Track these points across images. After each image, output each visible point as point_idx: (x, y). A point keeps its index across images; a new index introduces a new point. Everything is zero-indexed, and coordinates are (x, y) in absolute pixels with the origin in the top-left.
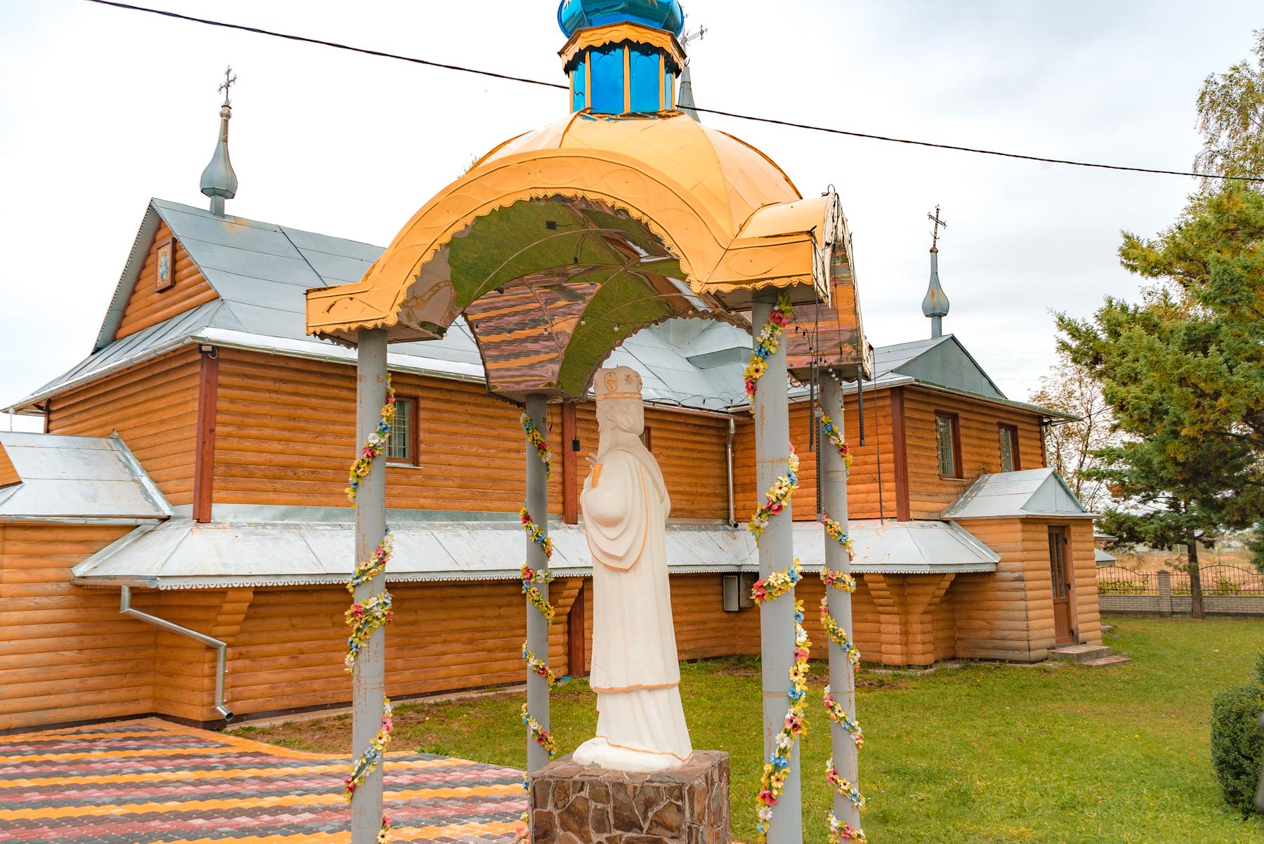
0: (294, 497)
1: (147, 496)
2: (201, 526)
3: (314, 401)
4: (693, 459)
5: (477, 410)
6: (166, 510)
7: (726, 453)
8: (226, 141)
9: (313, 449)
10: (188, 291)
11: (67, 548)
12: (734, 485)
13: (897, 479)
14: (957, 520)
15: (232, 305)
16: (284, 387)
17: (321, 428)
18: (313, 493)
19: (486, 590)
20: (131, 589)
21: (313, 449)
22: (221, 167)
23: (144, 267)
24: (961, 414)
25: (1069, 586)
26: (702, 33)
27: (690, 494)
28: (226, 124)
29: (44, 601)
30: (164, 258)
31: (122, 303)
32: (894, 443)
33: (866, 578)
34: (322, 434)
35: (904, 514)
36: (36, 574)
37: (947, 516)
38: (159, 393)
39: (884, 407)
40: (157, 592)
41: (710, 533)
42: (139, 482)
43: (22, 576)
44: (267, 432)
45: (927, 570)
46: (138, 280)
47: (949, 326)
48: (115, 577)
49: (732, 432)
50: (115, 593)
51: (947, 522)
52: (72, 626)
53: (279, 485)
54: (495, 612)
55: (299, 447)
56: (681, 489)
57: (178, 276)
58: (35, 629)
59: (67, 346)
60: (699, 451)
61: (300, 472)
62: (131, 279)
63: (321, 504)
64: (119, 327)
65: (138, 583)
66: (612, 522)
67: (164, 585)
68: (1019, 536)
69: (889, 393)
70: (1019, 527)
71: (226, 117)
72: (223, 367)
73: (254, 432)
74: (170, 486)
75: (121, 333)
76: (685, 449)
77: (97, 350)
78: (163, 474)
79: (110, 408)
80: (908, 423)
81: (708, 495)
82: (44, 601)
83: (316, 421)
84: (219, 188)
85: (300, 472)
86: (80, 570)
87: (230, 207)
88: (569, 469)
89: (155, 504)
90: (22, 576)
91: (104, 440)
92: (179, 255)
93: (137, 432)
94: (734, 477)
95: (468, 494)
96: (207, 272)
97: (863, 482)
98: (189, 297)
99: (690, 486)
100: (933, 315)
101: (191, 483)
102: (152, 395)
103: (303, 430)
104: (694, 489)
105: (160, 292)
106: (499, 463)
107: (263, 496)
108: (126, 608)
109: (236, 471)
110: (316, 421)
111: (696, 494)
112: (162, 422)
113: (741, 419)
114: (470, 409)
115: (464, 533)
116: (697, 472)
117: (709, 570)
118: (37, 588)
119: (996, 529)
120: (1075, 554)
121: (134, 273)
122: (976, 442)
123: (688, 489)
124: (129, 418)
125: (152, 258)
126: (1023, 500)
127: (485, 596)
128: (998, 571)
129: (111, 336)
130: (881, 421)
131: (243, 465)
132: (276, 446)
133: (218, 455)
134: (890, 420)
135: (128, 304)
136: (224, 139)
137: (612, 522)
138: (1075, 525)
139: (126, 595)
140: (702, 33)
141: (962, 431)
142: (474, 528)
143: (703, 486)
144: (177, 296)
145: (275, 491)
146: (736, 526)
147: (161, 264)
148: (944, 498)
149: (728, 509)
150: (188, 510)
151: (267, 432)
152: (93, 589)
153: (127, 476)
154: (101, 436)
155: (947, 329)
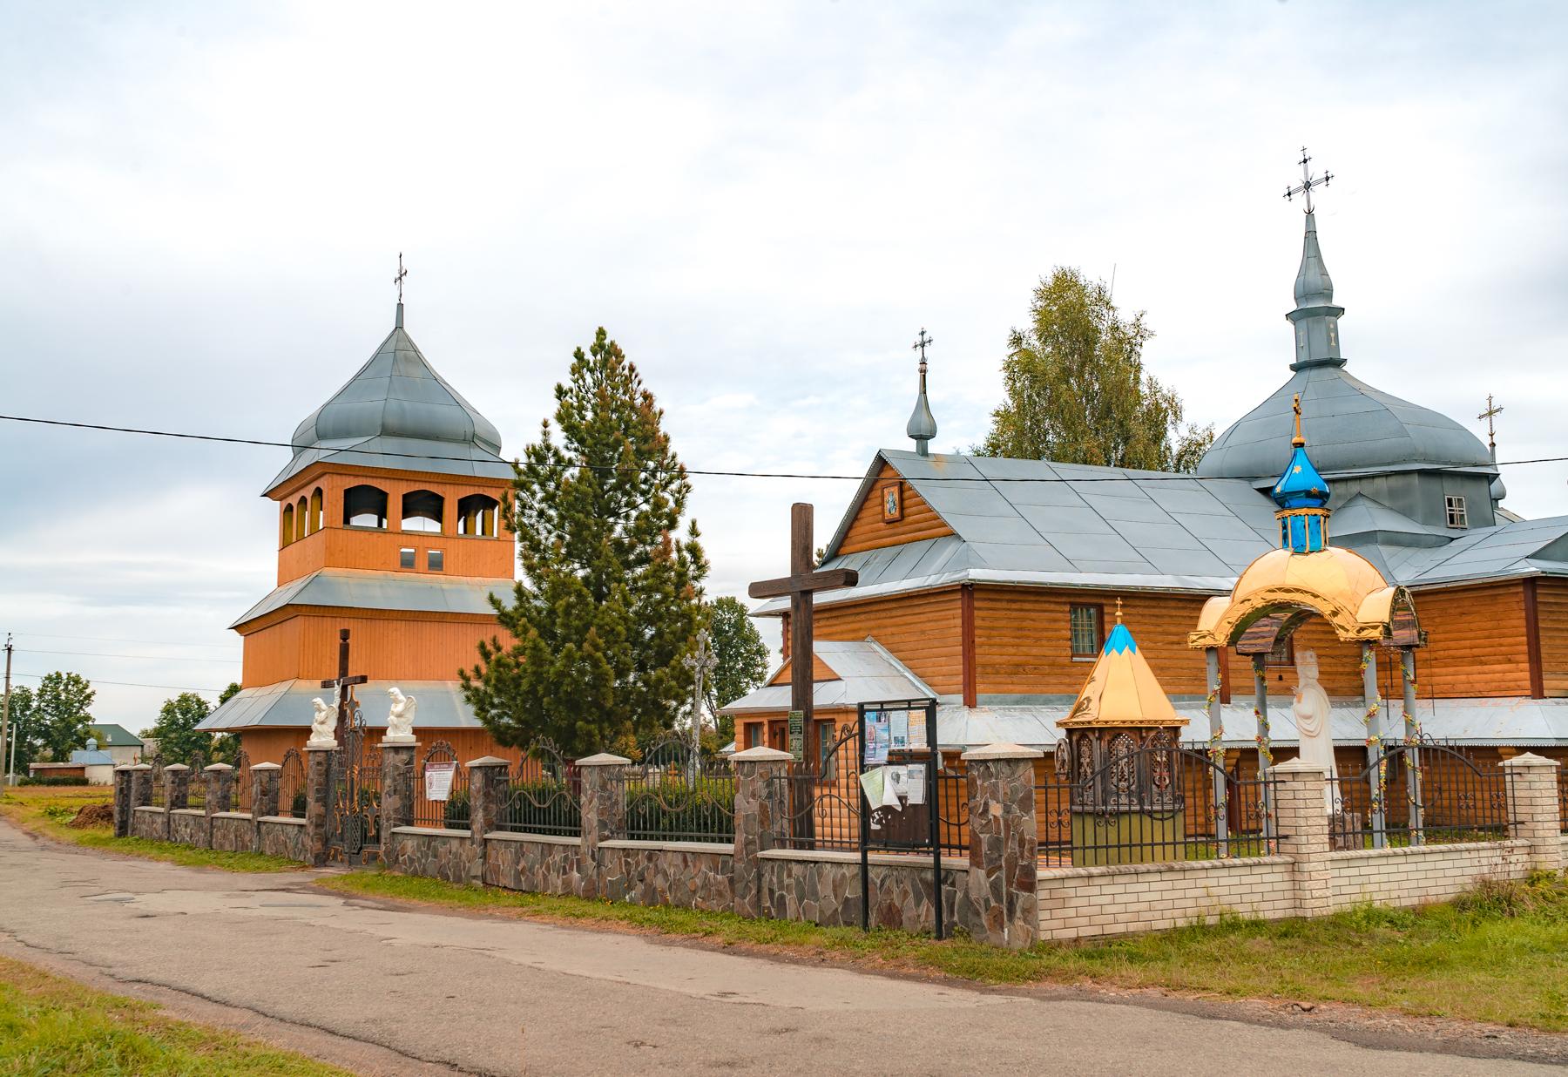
3: (1033, 615)
5: (1146, 611)
9: (1035, 651)
13: (1530, 661)
16: (1014, 606)
17: (1038, 635)
21: (1035, 651)
30: (891, 496)
32: (1527, 627)
34: (1039, 639)
35: (1538, 693)
38: (917, 610)
44: (1006, 640)
45: (1553, 743)
53: (1015, 679)
57: (907, 511)
71: (923, 372)
72: (976, 595)
73: (997, 640)
74: (937, 680)
75: (843, 550)
80: (1541, 608)
84: (922, 436)
87: (933, 446)
92: (907, 494)
93: (896, 639)
97: (1499, 663)
103: (1028, 637)
105: (889, 523)
106: (1165, 654)
109: (989, 670)
111: (1337, 673)
114: (1141, 611)
117: (1351, 744)
130: (1515, 606)
131: (993, 665)
132: (1012, 650)
133: (978, 659)
144: (901, 530)
151: (1006, 640)
154: (853, 640)
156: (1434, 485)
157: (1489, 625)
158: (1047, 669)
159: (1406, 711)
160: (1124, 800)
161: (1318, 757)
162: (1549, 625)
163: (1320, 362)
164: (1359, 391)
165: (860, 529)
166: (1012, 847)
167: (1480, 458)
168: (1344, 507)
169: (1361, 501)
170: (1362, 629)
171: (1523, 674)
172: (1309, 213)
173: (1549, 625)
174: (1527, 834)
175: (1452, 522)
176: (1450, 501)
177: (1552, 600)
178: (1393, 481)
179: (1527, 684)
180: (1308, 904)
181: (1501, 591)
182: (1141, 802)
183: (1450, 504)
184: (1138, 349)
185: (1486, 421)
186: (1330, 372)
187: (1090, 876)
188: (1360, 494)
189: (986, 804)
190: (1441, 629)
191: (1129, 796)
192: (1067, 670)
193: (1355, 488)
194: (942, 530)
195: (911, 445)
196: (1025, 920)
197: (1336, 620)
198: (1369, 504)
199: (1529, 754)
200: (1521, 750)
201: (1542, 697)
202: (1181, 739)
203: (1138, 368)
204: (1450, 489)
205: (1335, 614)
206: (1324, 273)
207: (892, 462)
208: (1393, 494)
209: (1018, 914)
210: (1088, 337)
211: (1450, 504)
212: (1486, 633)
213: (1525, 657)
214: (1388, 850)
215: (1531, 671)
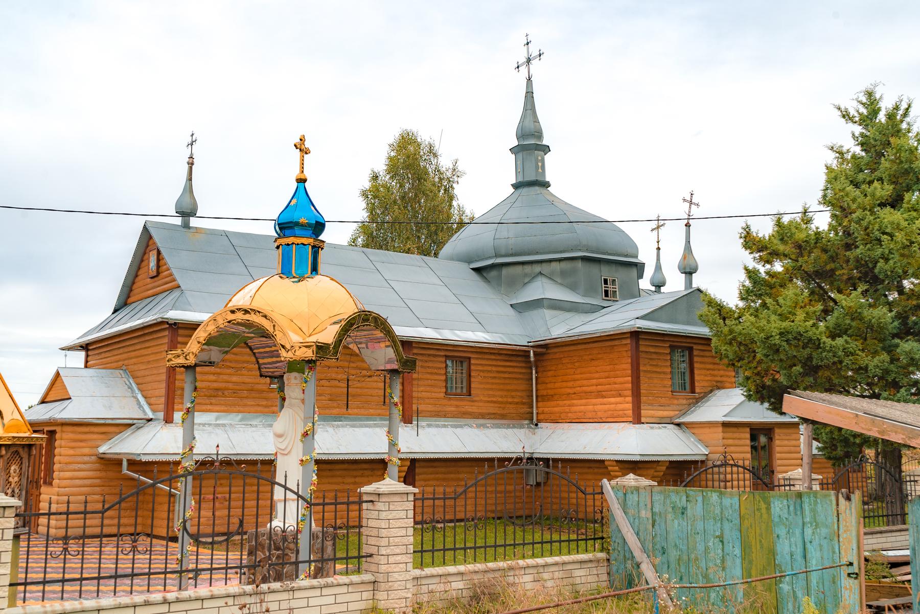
0: (223, 408)
1: (140, 406)
2: (168, 425)
4: (505, 378)
6: (150, 415)
7: (532, 373)
8: (190, 179)
9: (234, 379)
10: (167, 279)
11: (95, 436)
12: (537, 396)
14: (684, 423)
15: (187, 294)
18: (234, 405)
19: (346, 466)
20: (128, 460)
21: (234, 379)
22: (187, 198)
23: (142, 261)
24: (695, 347)
25: (773, 472)
27: (502, 403)
28: (191, 169)
29: (83, 466)
31: (129, 282)
33: (606, 463)
35: (637, 419)
36: (79, 451)
37: (678, 421)
38: (147, 345)
39: (626, 344)
40: (141, 463)
41: (515, 430)
42: (136, 398)
43: (71, 452)
45: (638, 458)
46: (139, 268)
47: (698, 281)
48: (120, 454)
49: (532, 359)
50: (119, 463)
51: (678, 425)
52: (97, 481)
53: (213, 400)
54: (352, 480)
55: (225, 377)
56: (494, 399)
58: (78, 482)
59: (95, 313)
60: (510, 373)
61: (226, 393)
62: (135, 268)
63: (239, 412)
64: (129, 297)
65: (130, 457)
67: (144, 459)
68: (721, 435)
69: (629, 335)
70: (720, 429)
72: (181, 332)
74: (153, 400)
75: (130, 300)
76: (498, 372)
77: (115, 311)
78: (149, 393)
79: (121, 351)
80: (642, 355)
81: (517, 403)
82: (83, 466)
83: (236, 362)
84: (187, 211)
85: (226, 393)
86: (102, 450)
87: (194, 222)
88: (407, 388)
89: (144, 411)
90: (71, 452)
91: (117, 371)
93: (136, 367)
94: (537, 390)
95: (335, 405)
96: (174, 271)
98: (166, 283)
99: (502, 397)
100: (685, 273)
101: (163, 400)
102: (143, 345)
104: (505, 400)
107: (204, 407)
108: (125, 471)
110: (236, 362)
111: (507, 403)
112: (149, 362)
113: (539, 350)
115: (330, 430)
116: (508, 387)
118: (79, 459)
119: (707, 430)
120: (778, 449)
121: (136, 264)
122: (711, 366)
123: (500, 399)
124: (131, 358)
125: (146, 256)
126: (727, 410)
127: (345, 470)
128: (707, 459)
129: (123, 304)
130: (625, 354)
132: (212, 378)
134: (629, 353)
135: (133, 283)
138: (780, 428)
139: (125, 463)
141: (696, 359)
142: (338, 426)
143: (513, 397)
144: (160, 282)
145: (211, 404)
146: (536, 425)
147: (148, 269)
148: (675, 407)
149: (532, 413)
150: (161, 415)
152: (109, 460)
153: (130, 394)
154: (116, 368)
155: (695, 285)
156: (594, 269)
157: (608, 368)
158: (245, 393)
161: (292, 472)
162: (649, 368)
163: (531, 183)
164: (553, 202)
167: (630, 251)
168: (529, 282)
171: (627, 405)
172: (529, 79)
173: (649, 368)
175: (606, 295)
176: (606, 281)
177: (652, 350)
178: (564, 265)
179: (630, 412)
181: (616, 343)
183: (606, 281)
184: (454, 185)
185: (655, 232)
186: (537, 189)
190: (578, 371)
192: (264, 395)
193: (537, 268)
198: (544, 280)
203: (451, 198)
204: (607, 272)
206: (536, 120)
207: (153, 232)
210: (420, 176)
212: (606, 374)
213: (629, 393)
215: (633, 402)
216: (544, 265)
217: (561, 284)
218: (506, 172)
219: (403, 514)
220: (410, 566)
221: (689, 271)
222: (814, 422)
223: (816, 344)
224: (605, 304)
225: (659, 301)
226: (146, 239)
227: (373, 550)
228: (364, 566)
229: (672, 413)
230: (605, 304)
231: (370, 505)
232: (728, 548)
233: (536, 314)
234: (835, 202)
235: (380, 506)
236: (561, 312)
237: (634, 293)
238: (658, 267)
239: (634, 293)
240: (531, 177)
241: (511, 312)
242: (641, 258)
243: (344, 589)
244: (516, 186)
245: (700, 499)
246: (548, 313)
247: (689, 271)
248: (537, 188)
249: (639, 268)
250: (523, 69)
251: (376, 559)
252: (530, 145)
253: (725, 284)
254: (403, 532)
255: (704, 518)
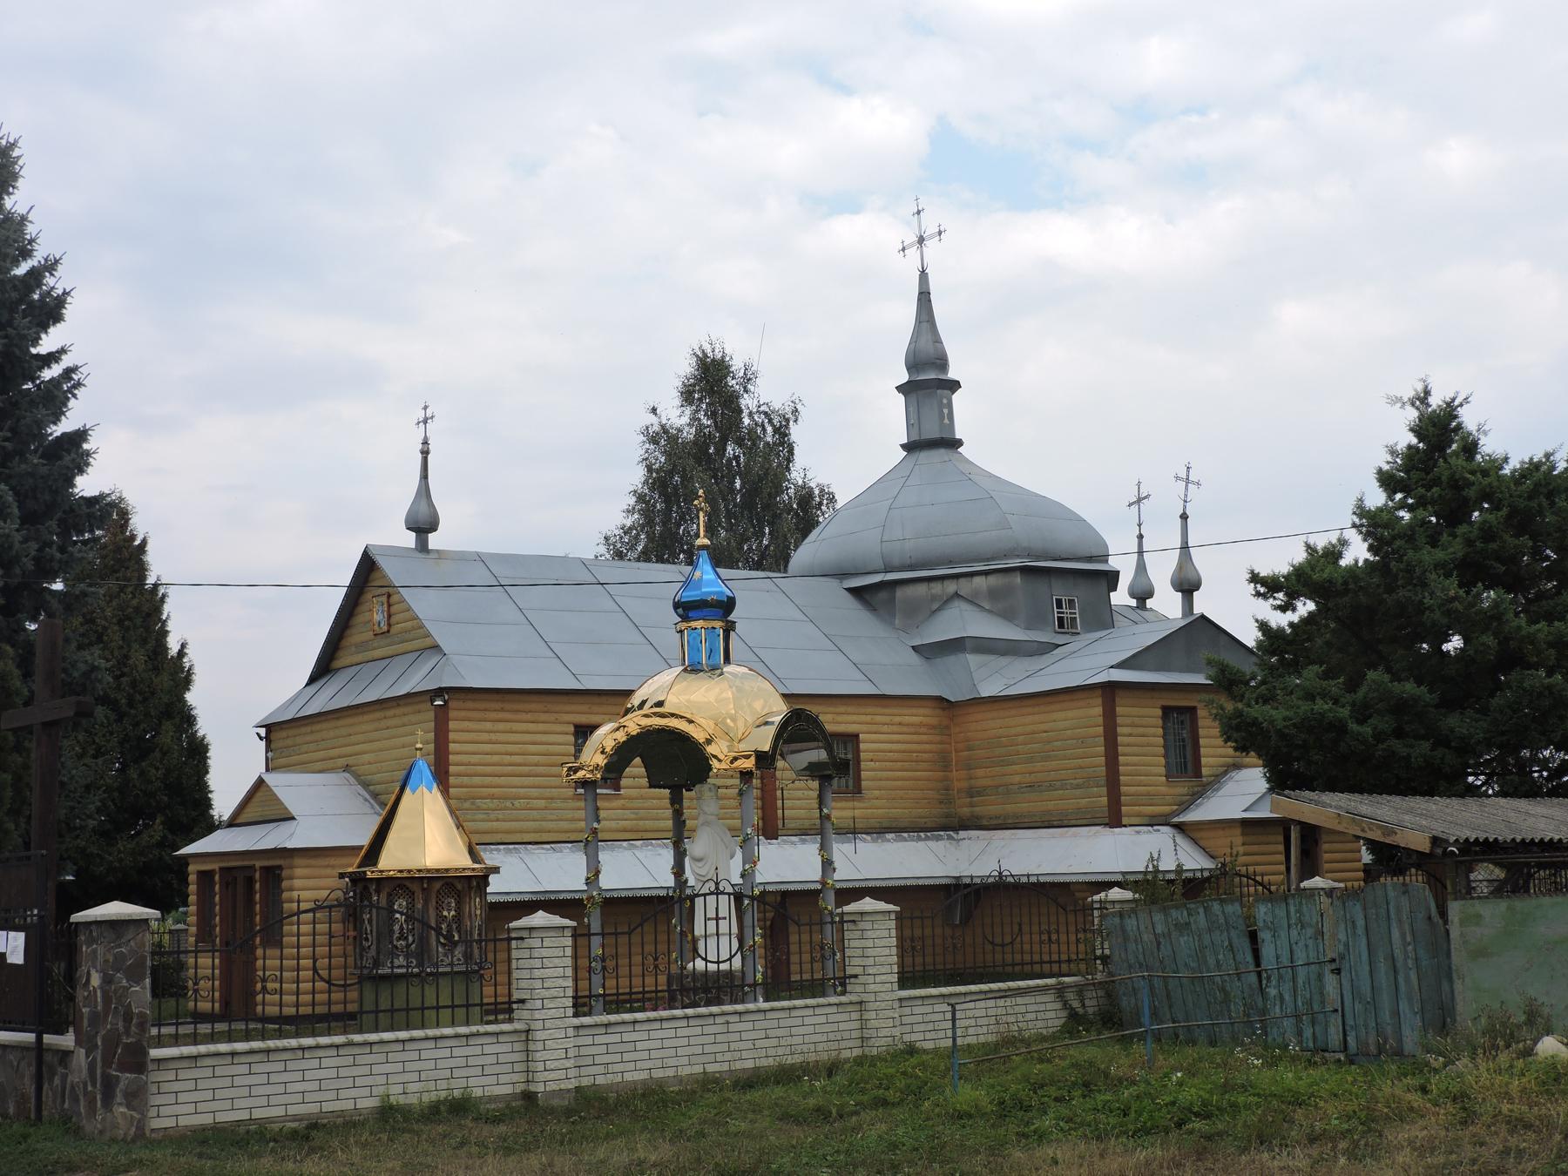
26: (940, 233)
37: (1176, 820)
47: (1203, 604)
57: (393, 620)
66: (699, 860)
70: (1238, 831)
71: (425, 453)
75: (336, 664)
77: (312, 680)
84: (423, 525)
87: (434, 540)
120: (1326, 856)
129: (324, 668)
136: (425, 475)
137: (699, 860)
140: (940, 233)
155: (1197, 610)
156: (1041, 586)
159: (822, 848)
160: (401, 960)
163: (932, 440)
164: (970, 475)
165: (357, 636)
166: (114, 1022)
168: (939, 609)
169: (957, 603)
170: (735, 759)
174: (859, 989)
175: (1061, 625)
180: (540, 1077)
182: (420, 965)
183: (1059, 605)
185: (1135, 508)
187: (303, 1049)
188: (957, 595)
189: (89, 974)
191: (407, 957)
193: (951, 587)
194: (428, 642)
195: (409, 540)
196: (129, 1106)
197: (710, 749)
198: (964, 606)
199: (1116, 889)
200: (1109, 885)
201: (1121, 825)
202: (489, 890)
204: (1060, 590)
205: (709, 742)
206: (937, 340)
207: (381, 561)
208: (993, 594)
209: (119, 1098)
211: (1059, 605)
214: (762, 1004)
216: (962, 581)
217: (989, 611)
218: (892, 420)
219: (886, 933)
220: (896, 986)
221: (1187, 586)
222: (1300, 823)
223: (1339, 728)
224: (1059, 639)
225: (1148, 636)
226: (368, 566)
227: (858, 971)
228: (849, 988)
229: (1167, 809)
230: (1059, 639)
231: (851, 926)
232: (1240, 957)
233: (952, 661)
234: (1373, 524)
235: (862, 925)
236: (992, 657)
237: (1103, 618)
238: (1141, 568)
239: (1103, 618)
240: (931, 432)
241: (915, 658)
242: (1114, 563)
243: (834, 1009)
244: (909, 447)
245: (1201, 910)
246: (973, 659)
247: (1187, 586)
248: (942, 451)
249: (1112, 578)
250: (913, 253)
251: (861, 979)
252: (928, 381)
253: (1242, 616)
254: (887, 951)
255: (1210, 930)
